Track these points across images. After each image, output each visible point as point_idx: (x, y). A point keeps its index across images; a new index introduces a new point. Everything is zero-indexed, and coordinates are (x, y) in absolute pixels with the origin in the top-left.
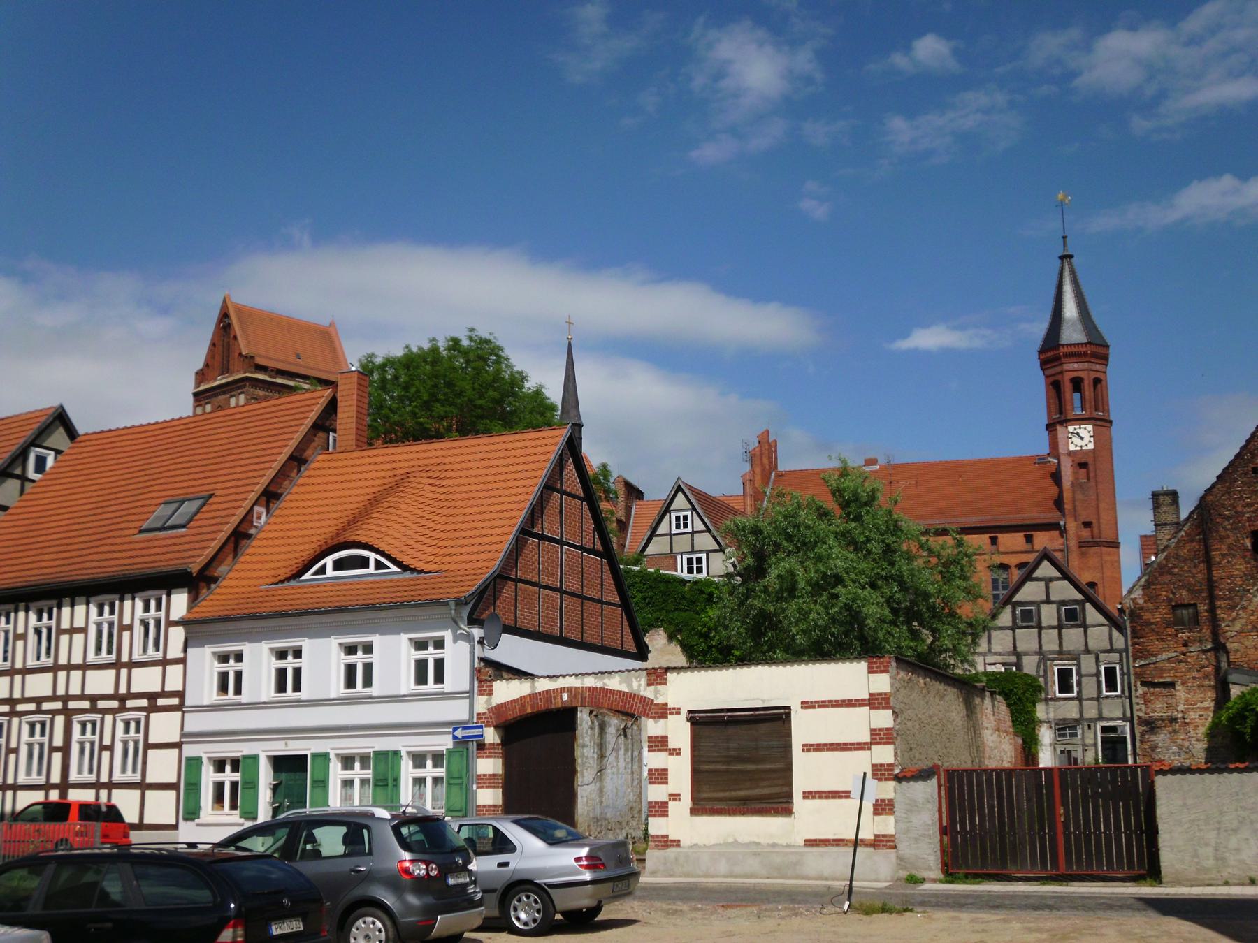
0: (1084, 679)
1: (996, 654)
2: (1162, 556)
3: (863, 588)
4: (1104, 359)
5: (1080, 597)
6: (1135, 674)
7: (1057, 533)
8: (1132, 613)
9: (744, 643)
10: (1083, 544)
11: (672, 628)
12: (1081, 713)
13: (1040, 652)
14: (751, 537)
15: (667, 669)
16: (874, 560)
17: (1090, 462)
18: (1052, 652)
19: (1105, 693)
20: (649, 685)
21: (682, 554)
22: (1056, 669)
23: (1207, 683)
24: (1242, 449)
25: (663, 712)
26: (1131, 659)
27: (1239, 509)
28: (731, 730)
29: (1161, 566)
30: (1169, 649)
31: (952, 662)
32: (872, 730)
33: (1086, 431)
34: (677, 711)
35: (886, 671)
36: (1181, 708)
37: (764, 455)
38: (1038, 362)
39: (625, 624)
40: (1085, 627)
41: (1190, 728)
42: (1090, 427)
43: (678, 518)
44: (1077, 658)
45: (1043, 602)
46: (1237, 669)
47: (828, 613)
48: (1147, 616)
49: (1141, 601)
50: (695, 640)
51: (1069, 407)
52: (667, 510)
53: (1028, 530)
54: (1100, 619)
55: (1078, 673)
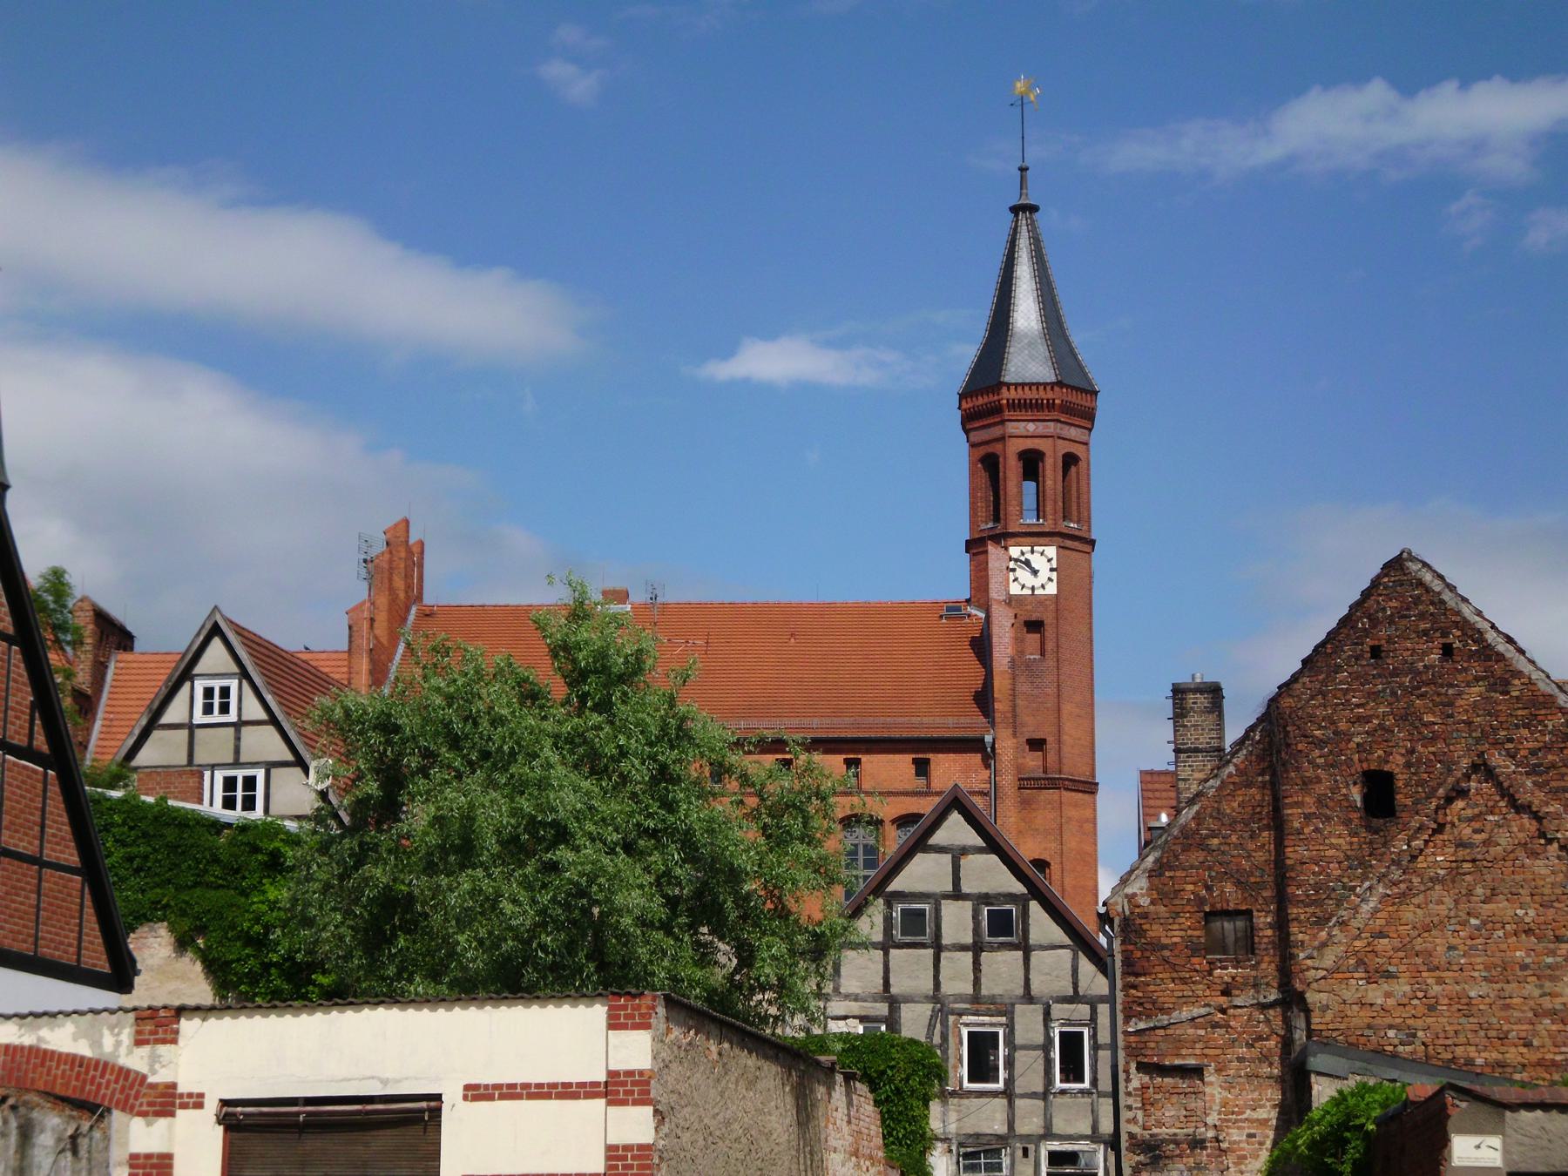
0: (1018, 1055)
1: (847, 997)
2: (1188, 814)
3: (612, 852)
4: (1087, 417)
5: (1019, 888)
6: (1126, 1048)
7: (976, 758)
8: (1126, 921)
9: (347, 957)
10: (1026, 783)
11: (186, 924)
12: (1011, 1124)
13: (936, 997)
14: (375, 738)
15: (181, 1011)
16: (634, 796)
17: (1049, 620)
18: (960, 998)
19: (1058, 1085)
20: (139, 1043)
21: (213, 767)
22: (965, 1032)
23: (1265, 1070)
24: (1355, 607)
25: (166, 1101)
26: (1120, 1017)
27: (1342, 726)
28: (313, 1144)
29: (1185, 832)
30: (1194, 999)
31: (773, 1011)
32: (611, 1149)
33: (1045, 557)
34: (197, 1101)
35: (646, 1026)
36: (1212, 1119)
37: (397, 566)
38: (957, 416)
39: (89, 911)
40: (1026, 949)
41: (1230, 1160)
42: (1051, 551)
43: (209, 693)
44: (1008, 1012)
45: (946, 896)
46: (1327, 1045)
47: (534, 901)
48: (1155, 931)
49: (1144, 901)
50: (235, 951)
51: (1013, 509)
52: (186, 675)
53: (921, 749)
54: (1057, 934)
55: (1010, 1042)
